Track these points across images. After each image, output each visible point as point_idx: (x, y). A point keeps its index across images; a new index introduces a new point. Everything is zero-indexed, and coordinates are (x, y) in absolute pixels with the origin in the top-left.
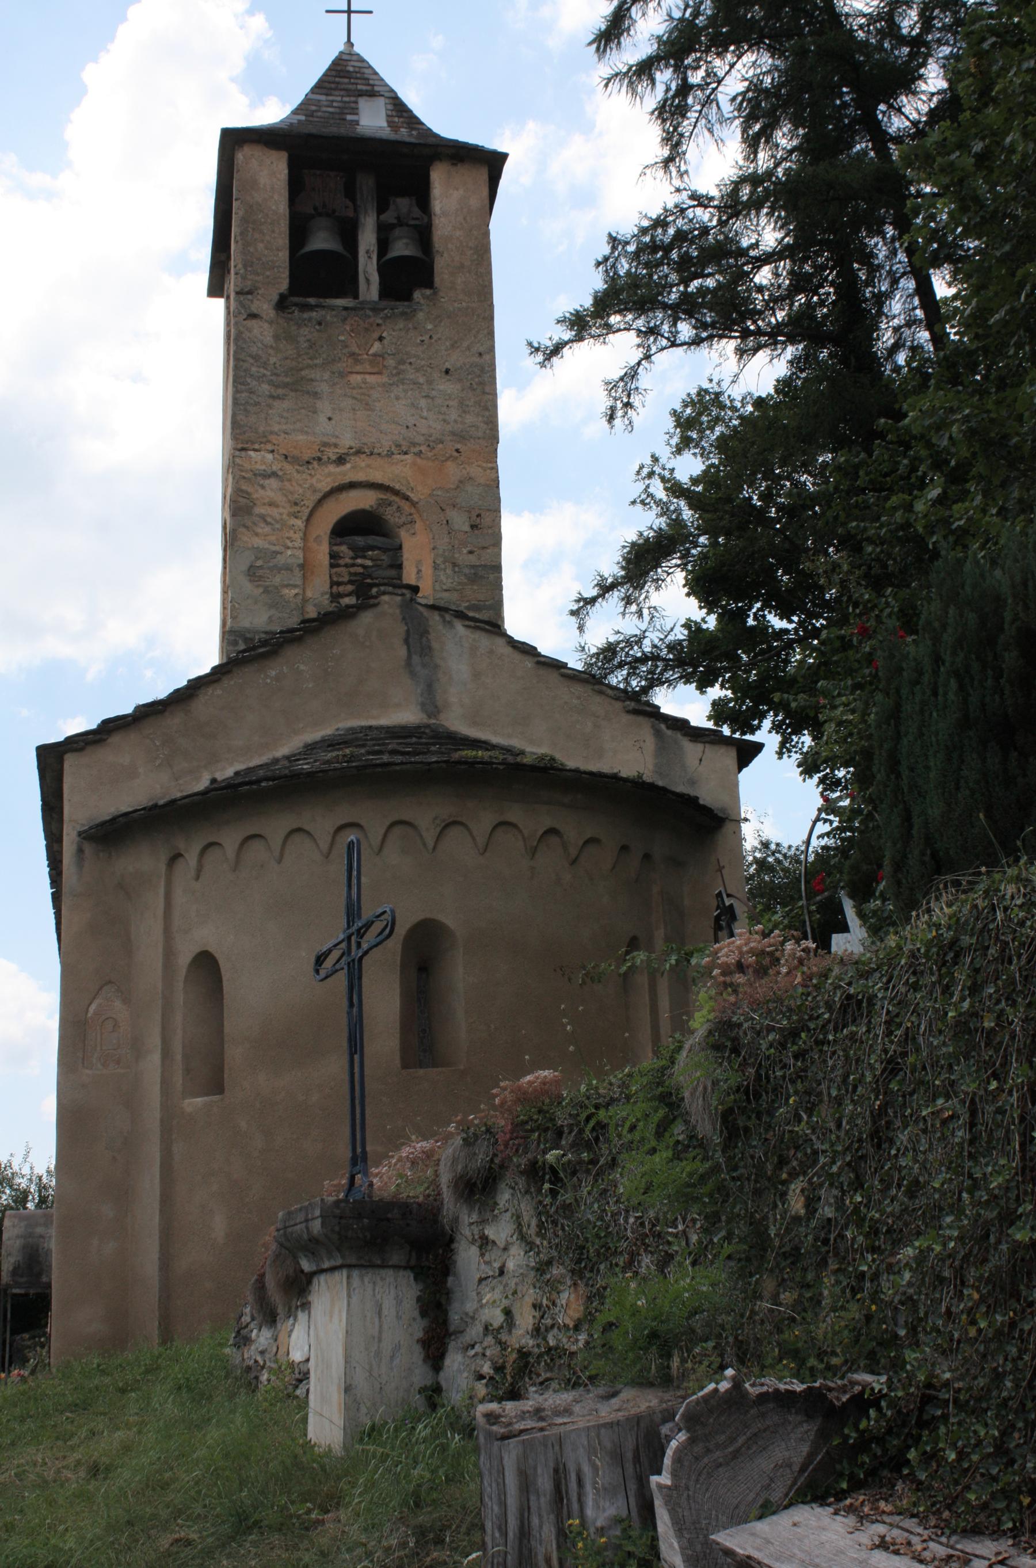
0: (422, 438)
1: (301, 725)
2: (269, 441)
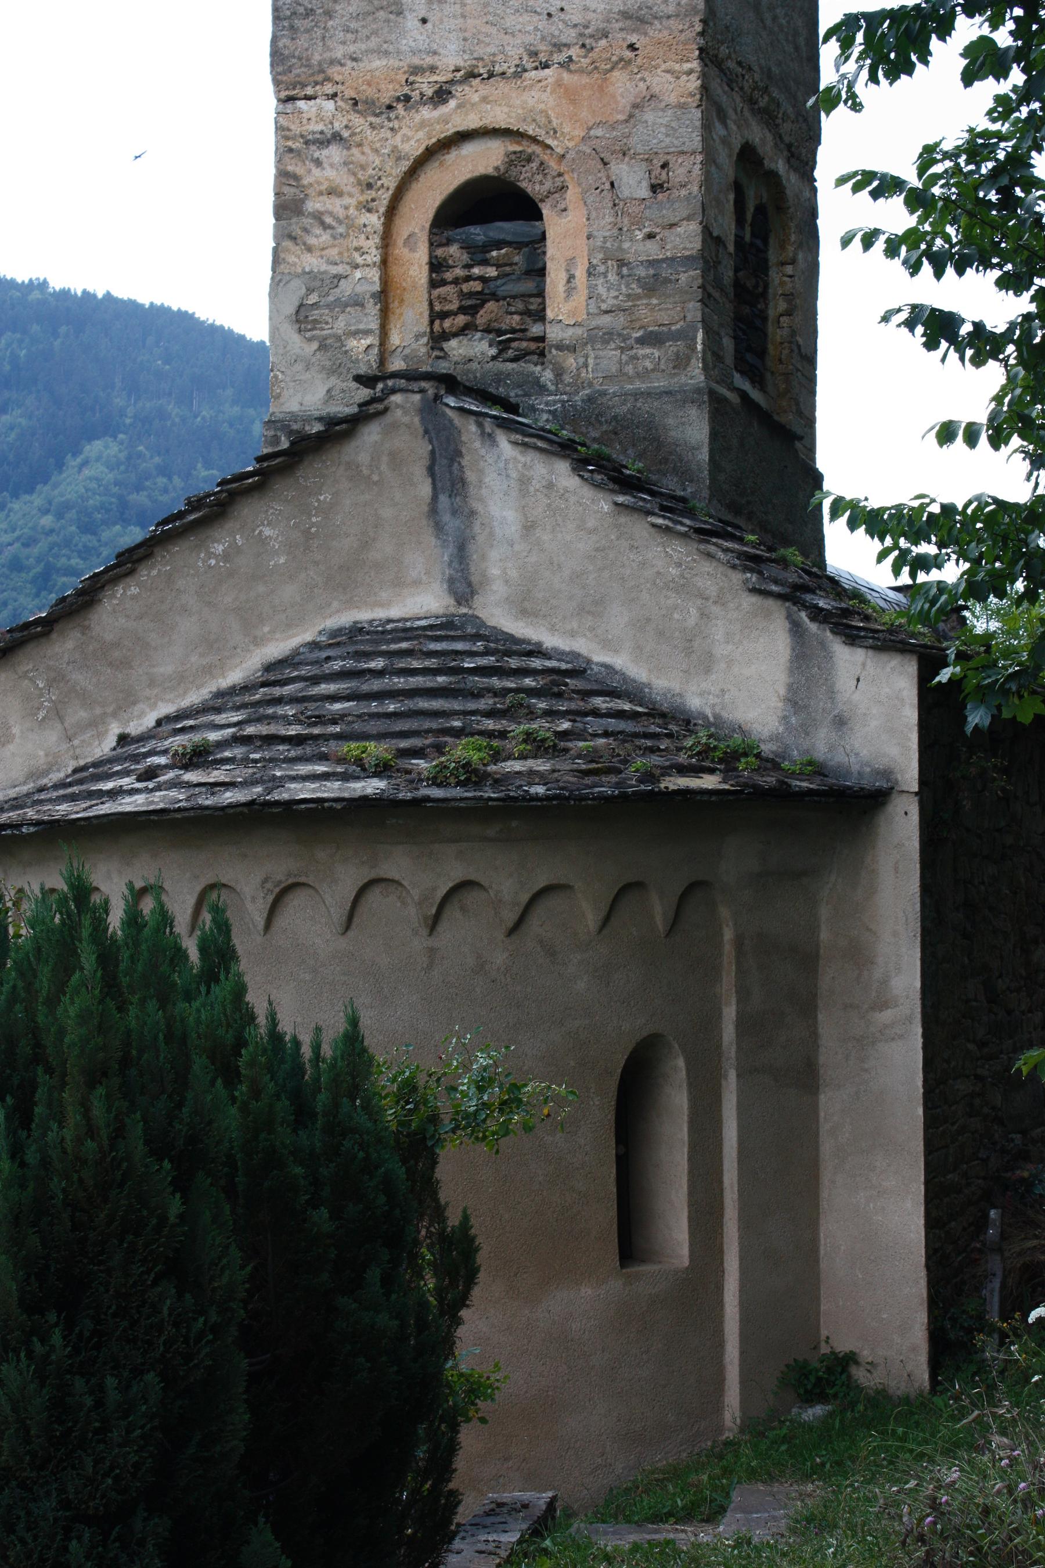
0: (573, 33)
1: (266, 629)
2: (328, 79)
